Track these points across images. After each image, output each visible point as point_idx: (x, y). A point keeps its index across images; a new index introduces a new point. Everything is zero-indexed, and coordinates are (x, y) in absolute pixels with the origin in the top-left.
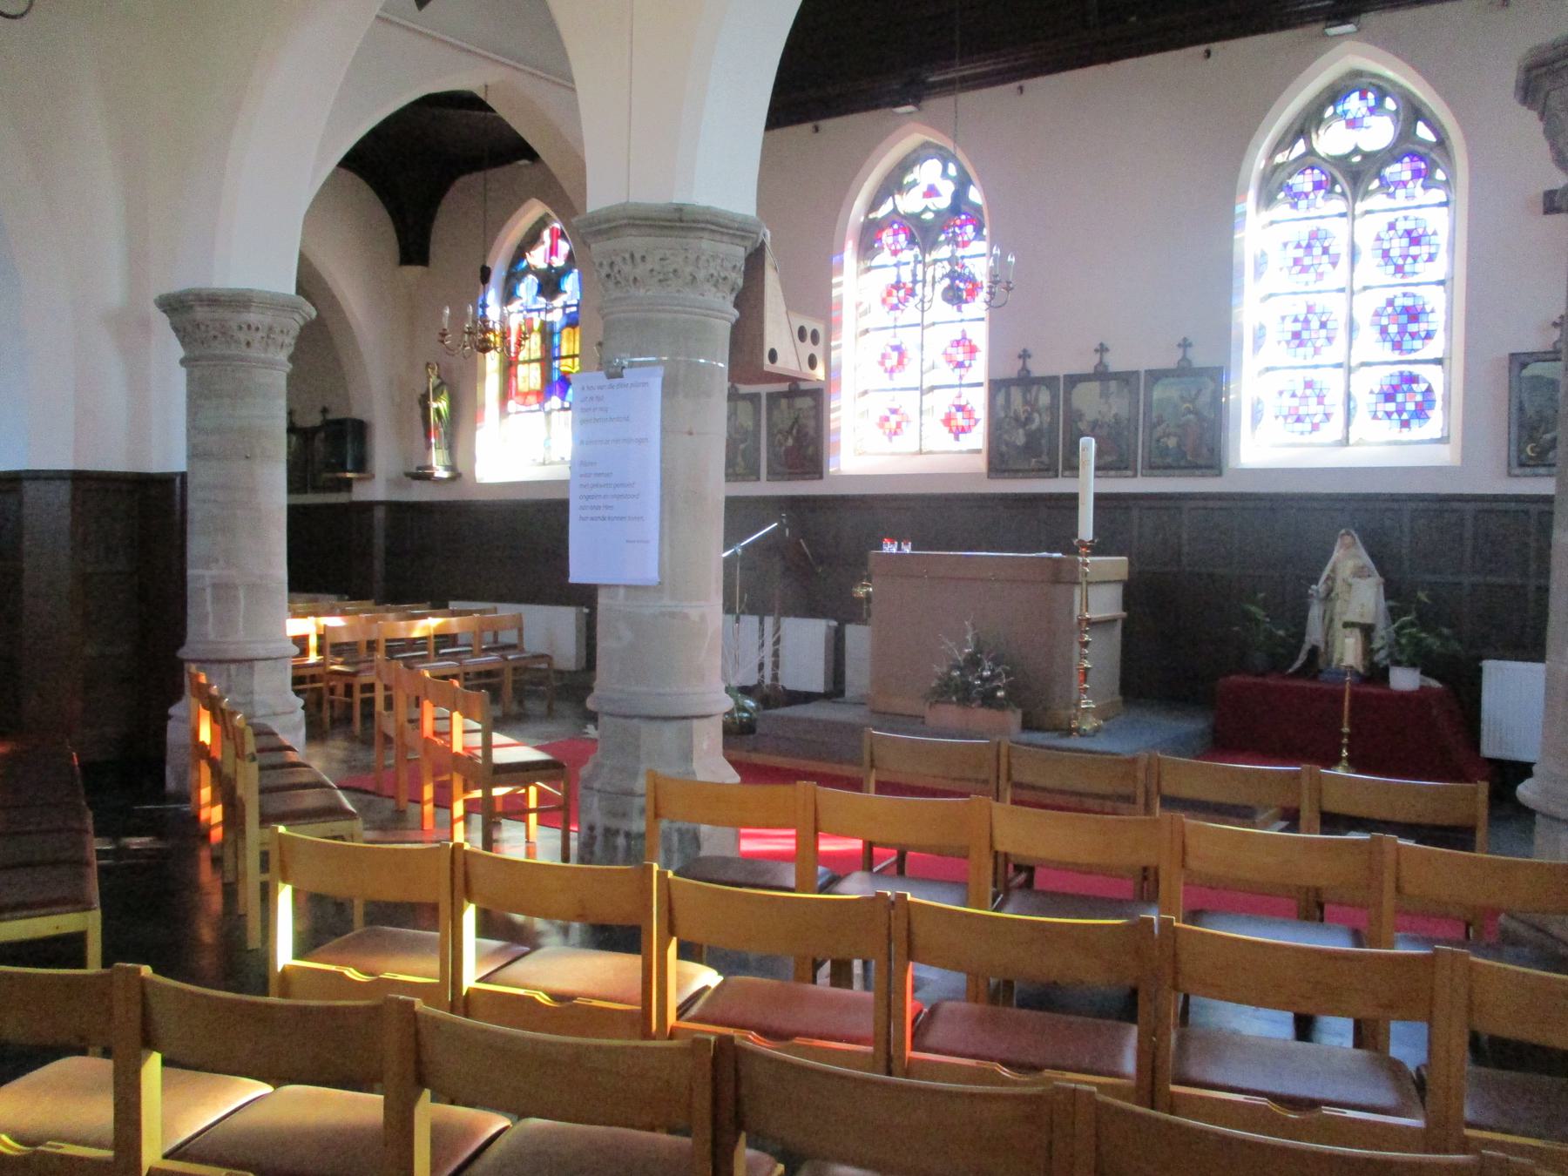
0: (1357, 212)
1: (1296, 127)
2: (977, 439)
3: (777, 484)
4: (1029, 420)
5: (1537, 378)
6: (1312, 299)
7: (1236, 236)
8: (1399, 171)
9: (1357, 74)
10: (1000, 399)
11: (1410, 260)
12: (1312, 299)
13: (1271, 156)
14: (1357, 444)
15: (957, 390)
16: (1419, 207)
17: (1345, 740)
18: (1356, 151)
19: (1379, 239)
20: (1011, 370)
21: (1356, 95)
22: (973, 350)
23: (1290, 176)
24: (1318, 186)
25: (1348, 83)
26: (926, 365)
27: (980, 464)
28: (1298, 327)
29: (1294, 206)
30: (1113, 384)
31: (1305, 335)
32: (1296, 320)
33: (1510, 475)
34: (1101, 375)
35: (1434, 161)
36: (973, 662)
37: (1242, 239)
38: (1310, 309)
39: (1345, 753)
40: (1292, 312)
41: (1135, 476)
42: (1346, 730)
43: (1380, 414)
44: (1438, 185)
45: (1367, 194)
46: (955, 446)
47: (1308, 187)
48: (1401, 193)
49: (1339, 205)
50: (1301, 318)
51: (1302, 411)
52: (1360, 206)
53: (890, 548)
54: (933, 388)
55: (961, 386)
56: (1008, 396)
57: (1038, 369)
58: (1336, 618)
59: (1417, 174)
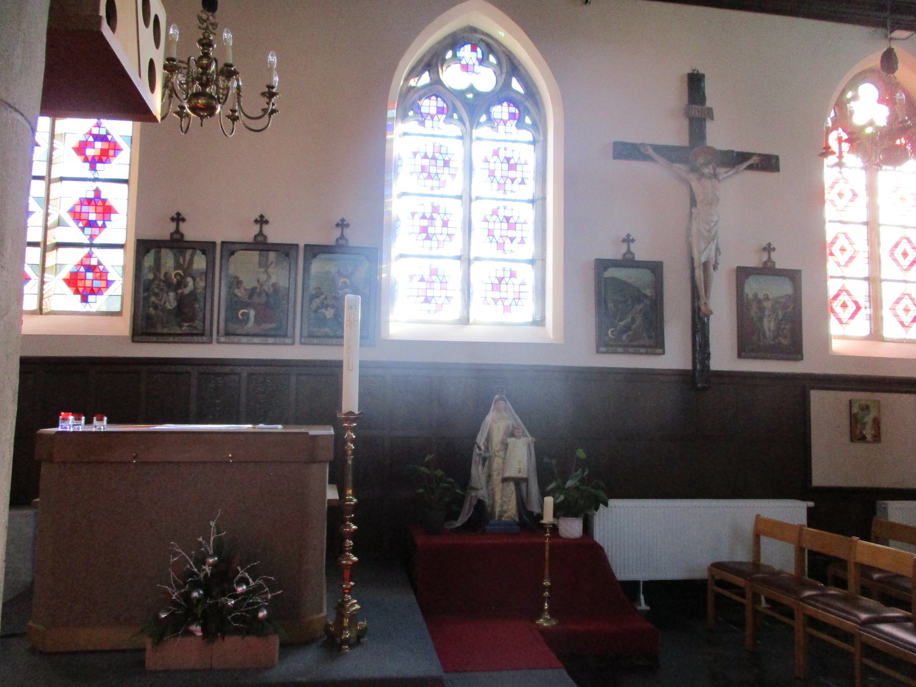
0: (474, 137)
1: (426, 60)
2: (115, 297)
3: (139, 345)
4: (181, 284)
5: (614, 279)
6: (437, 201)
7: (388, 137)
8: (501, 111)
9: (473, 30)
10: (149, 260)
11: (509, 181)
12: (437, 201)
13: (407, 79)
14: (475, 324)
15: (86, 251)
16: (515, 141)
17: (547, 594)
18: (471, 89)
19: (486, 161)
20: (165, 231)
21: (468, 47)
22: (107, 211)
23: (420, 99)
24: (440, 111)
25: (466, 35)
26: (52, 220)
27: (124, 327)
28: (425, 223)
29: (422, 123)
30: (272, 255)
31: (431, 230)
32: (424, 217)
33: (598, 352)
34: (260, 245)
35: (526, 107)
36: (222, 578)
37: (392, 140)
38: (435, 210)
39: (546, 606)
40: (421, 210)
41: (210, 342)
42: (547, 583)
43: (489, 300)
44: (526, 127)
45: (479, 124)
46: (79, 306)
47: (433, 111)
48: (501, 128)
49: (455, 129)
50: (428, 216)
51: (430, 293)
52: (476, 133)
53: (70, 424)
54: (59, 245)
55: (91, 245)
56: (158, 260)
57: (191, 232)
58: (495, 474)
59: (512, 116)
